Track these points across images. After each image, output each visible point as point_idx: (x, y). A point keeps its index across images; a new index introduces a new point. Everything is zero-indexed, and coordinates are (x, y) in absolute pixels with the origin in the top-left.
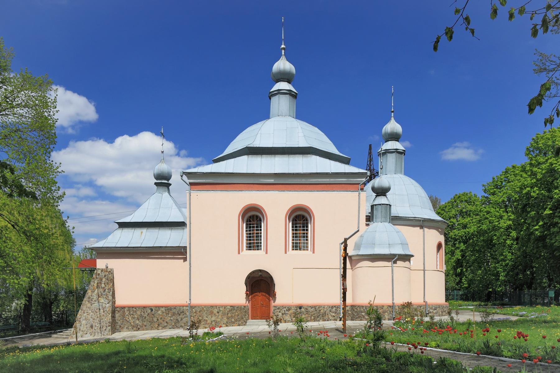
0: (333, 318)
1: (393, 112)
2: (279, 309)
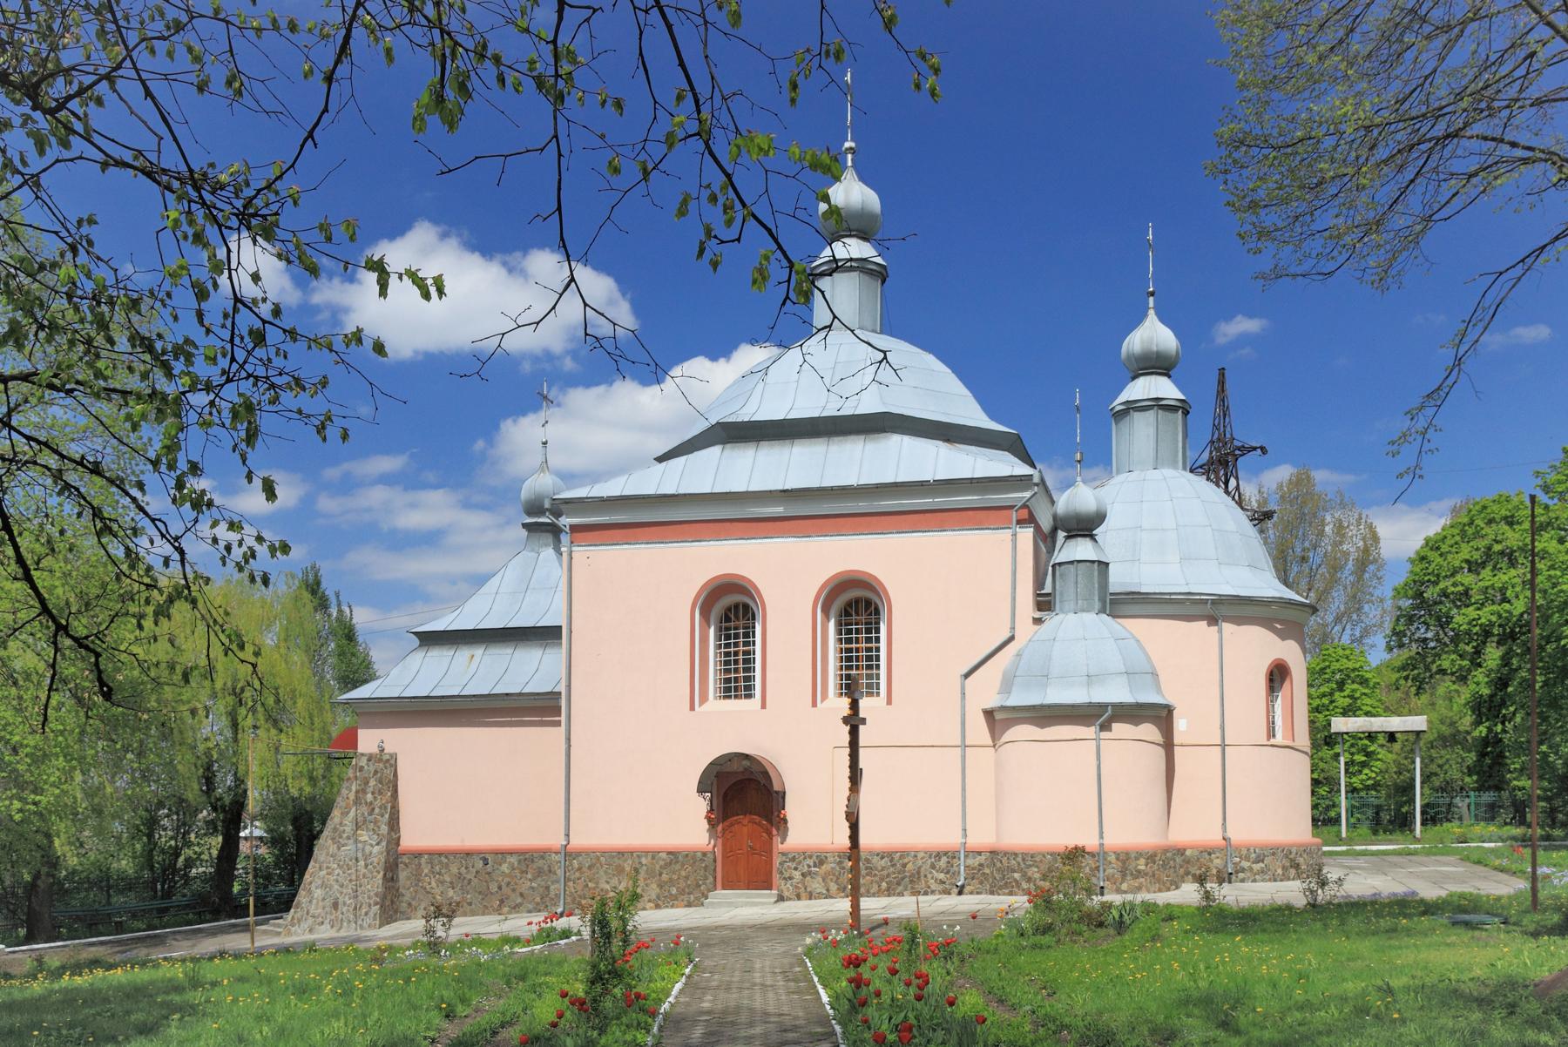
0: (941, 887)
1: (1152, 294)
2: (793, 859)
